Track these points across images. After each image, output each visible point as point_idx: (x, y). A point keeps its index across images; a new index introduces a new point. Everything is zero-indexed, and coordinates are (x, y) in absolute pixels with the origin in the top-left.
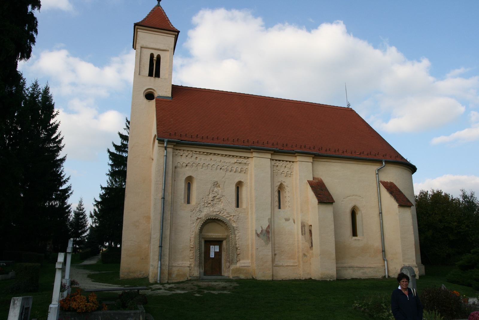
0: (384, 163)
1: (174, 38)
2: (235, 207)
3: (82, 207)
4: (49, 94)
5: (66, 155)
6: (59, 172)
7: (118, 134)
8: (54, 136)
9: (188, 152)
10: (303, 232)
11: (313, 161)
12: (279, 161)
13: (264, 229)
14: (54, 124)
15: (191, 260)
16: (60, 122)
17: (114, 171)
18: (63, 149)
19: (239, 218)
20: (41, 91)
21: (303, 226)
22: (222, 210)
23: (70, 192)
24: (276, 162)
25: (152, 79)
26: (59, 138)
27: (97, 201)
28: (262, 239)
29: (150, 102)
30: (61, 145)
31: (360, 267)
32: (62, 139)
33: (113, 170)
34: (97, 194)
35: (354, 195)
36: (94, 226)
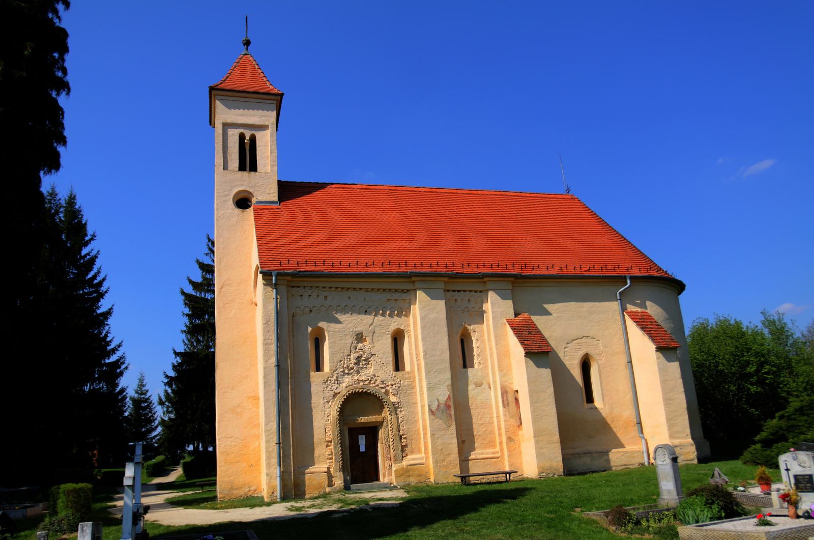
0: (628, 281)
1: (275, 105)
2: (394, 371)
3: (144, 389)
4: (77, 207)
5: (113, 306)
6: (102, 334)
7: (196, 263)
8: (90, 276)
9: (312, 289)
10: (506, 402)
11: (513, 286)
12: (459, 291)
13: (441, 402)
14: (89, 255)
16: (99, 253)
17: (193, 325)
18: (107, 296)
19: (400, 389)
20: (63, 203)
21: (504, 393)
22: (372, 378)
23: (123, 367)
24: (455, 293)
25: (245, 174)
26: (99, 279)
27: (170, 377)
28: (440, 419)
29: (245, 213)
30: (102, 289)
31: (603, 452)
32: (104, 280)
33: (192, 322)
34: (167, 364)
35: (583, 337)
36: (166, 419)
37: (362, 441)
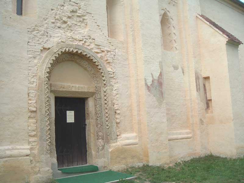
13: (155, 78)
15: (31, 139)
37: (70, 116)
